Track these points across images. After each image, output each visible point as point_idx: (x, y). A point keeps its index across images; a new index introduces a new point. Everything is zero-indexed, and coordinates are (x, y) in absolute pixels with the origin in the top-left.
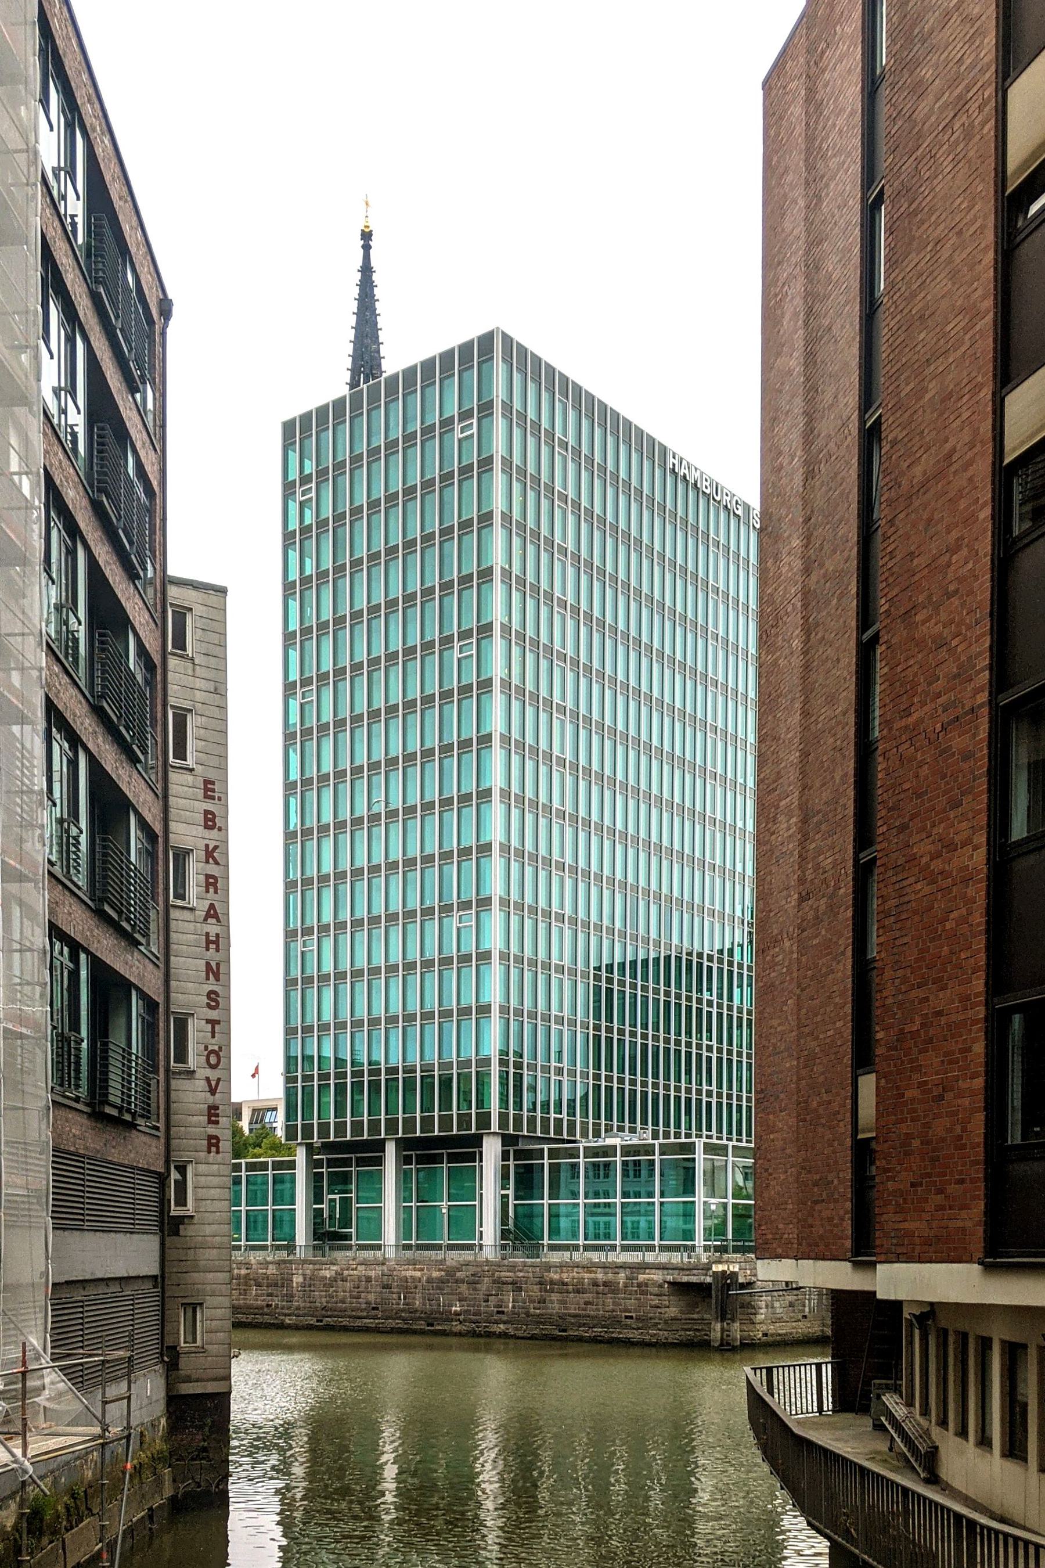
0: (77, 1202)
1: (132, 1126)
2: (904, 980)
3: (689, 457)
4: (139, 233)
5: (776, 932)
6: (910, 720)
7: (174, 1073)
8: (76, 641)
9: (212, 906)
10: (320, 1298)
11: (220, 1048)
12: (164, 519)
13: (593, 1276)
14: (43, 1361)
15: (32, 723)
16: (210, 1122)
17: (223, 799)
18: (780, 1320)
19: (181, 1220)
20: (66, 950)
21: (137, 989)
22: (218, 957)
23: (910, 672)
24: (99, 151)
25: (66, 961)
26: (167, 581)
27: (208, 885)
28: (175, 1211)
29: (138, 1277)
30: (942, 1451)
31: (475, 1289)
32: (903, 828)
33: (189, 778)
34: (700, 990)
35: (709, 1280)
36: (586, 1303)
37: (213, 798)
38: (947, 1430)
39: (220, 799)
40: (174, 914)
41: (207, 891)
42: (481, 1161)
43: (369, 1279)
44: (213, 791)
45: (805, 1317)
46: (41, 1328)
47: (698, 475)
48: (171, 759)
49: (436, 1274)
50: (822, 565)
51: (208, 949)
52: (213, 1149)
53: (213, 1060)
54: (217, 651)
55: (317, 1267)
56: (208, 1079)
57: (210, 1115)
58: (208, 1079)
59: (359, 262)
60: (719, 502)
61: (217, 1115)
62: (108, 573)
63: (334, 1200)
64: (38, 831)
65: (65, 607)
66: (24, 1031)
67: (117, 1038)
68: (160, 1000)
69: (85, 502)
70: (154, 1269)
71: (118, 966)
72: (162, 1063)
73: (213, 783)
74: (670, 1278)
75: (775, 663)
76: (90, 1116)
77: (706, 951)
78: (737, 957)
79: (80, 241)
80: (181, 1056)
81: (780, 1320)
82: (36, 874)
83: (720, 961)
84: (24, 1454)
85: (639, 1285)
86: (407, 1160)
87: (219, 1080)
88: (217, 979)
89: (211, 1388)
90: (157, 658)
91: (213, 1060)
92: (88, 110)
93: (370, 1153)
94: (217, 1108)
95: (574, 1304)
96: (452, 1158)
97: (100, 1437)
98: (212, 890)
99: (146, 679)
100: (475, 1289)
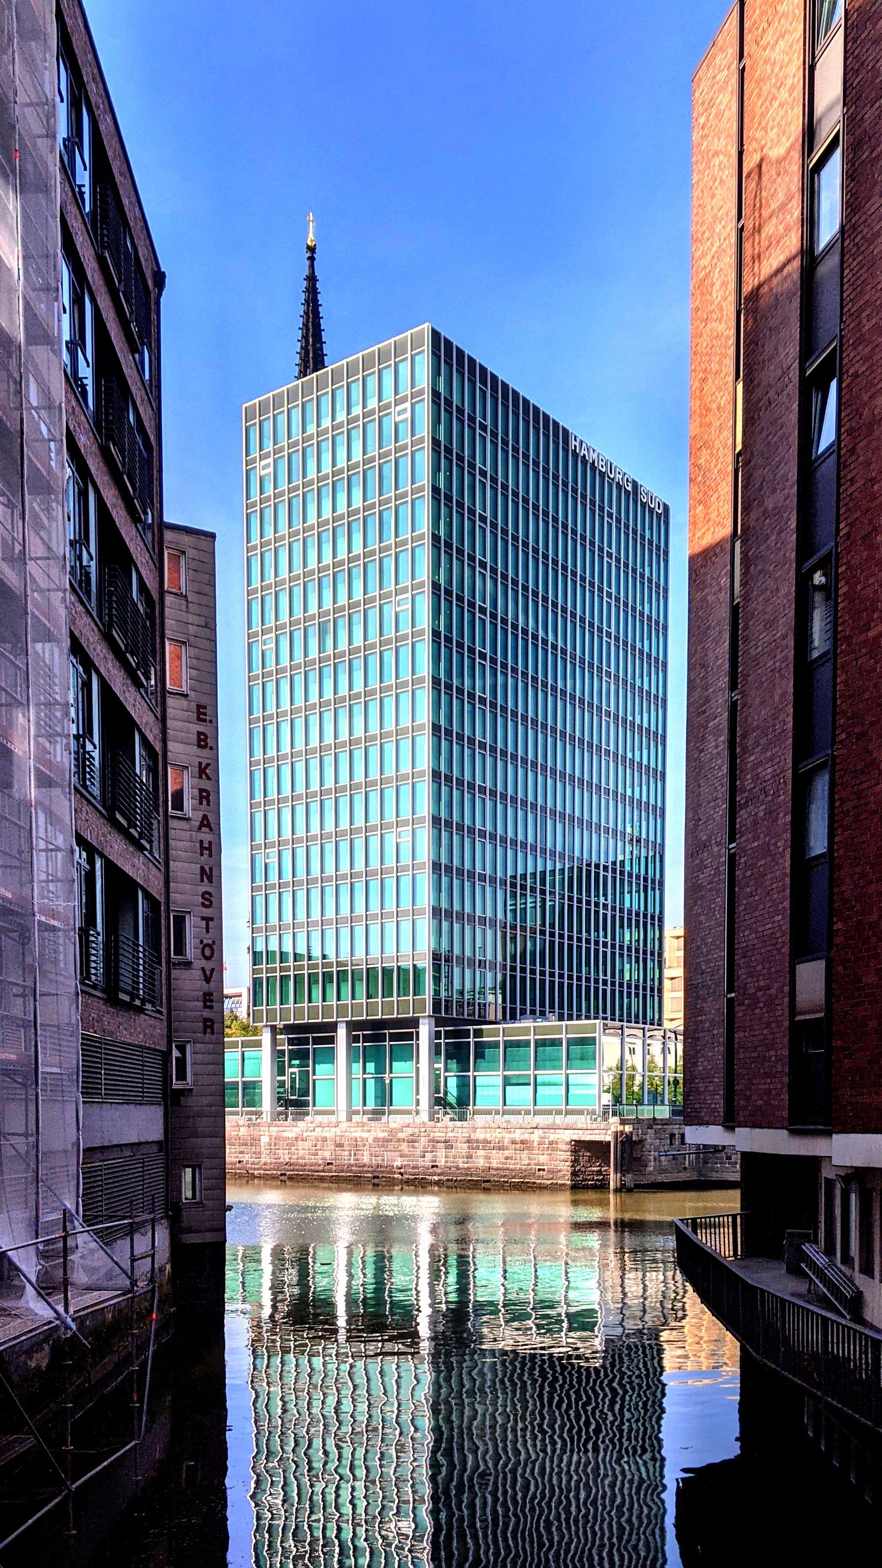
0: (101, 1075)
1: (141, 1010)
2: (863, 875)
3: (588, 441)
4: (137, 209)
5: (704, 838)
6: (871, 634)
7: (174, 964)
8: (88, 574)
9: (205, 817)
10: (285, 1157)
11: (214, 942)
12: (160, 471)
13: (512, 1136)
14: (76, 1223)
15: (58, 641)
16: (205, 1006)
17: (213, 722)
18: (666, 1171)
19: (181, 1092)
20: (84, 855)
21: (144, 891)
22: (212, 861)
23: (869, 590)
24: (102, 127)
25: (85, 864)
26: (163, 526)
27: (201, 798)
28: (176, 1085)
29: (147, 1143)
30: (868, 1296)
31: (413, 1147)
32: (863, 734)
33: (184, 703)
34: (597, 896)
35: (609, 1138)
36: (507, 1158)
37: (205, 721)
38: (873, 1278)
39: (211, 721)
40: (173, 823)
41: (201, 803)
42: (418, 1039)
43: (325, 1140)
44: (205, 714)
45: (685, 1169)
46: (73, 1189)
47: (595, 456)
48: (168, 686)
49: (381, 1135)
50: (761, 503)
51: (202, 854)
52: (209, 1030)
53: (207, 952)
54: (207, 589)
55: (281, 1129)
56: (203, 969)
57: (205, 1001)
58: (203, 969)
59: (306, 272)
60: (613, 479)
61: (212, 1001)
62: (114, 514)
63: (294, 1073)
64: (65, 741)
65: (79, 542)
66: (56, 923)
67: (126, 933)
68: (162, 900)
69: (95, 449)
70: (162, 1138)
71: (128, 869)
72: (164, 955)
73: (205, 707)
74: (576, 1138)
75: (704, 599)
76: (106, 1001)
77: (602, 863)
78: (627, 868)
79: (87, 209)
80: (180, 948)
81: (666, 1171)
82: (63, 779)
83: (614, 871)
84: (66, 1311)
85: (551, 1143)
86: (356, 1039)
87: (213, 970)
88: (210, 881)
89: (209, 1237)
90: (155, 596)
91: (207, 952)
92: (92, 88)
93: (324, 1033)
94: (211, 994)
95: (497, 1160)
96: (394, 1037)
97: (130, 1291)
98: (205, 802)
99: (146, 612)
100: (413, 1147)
